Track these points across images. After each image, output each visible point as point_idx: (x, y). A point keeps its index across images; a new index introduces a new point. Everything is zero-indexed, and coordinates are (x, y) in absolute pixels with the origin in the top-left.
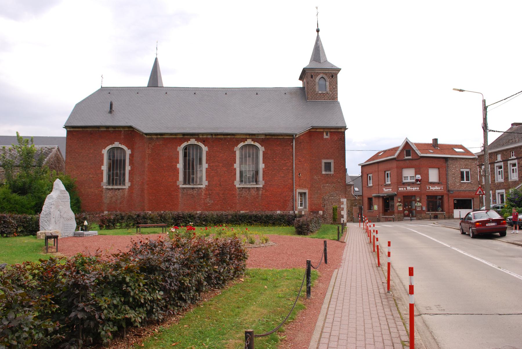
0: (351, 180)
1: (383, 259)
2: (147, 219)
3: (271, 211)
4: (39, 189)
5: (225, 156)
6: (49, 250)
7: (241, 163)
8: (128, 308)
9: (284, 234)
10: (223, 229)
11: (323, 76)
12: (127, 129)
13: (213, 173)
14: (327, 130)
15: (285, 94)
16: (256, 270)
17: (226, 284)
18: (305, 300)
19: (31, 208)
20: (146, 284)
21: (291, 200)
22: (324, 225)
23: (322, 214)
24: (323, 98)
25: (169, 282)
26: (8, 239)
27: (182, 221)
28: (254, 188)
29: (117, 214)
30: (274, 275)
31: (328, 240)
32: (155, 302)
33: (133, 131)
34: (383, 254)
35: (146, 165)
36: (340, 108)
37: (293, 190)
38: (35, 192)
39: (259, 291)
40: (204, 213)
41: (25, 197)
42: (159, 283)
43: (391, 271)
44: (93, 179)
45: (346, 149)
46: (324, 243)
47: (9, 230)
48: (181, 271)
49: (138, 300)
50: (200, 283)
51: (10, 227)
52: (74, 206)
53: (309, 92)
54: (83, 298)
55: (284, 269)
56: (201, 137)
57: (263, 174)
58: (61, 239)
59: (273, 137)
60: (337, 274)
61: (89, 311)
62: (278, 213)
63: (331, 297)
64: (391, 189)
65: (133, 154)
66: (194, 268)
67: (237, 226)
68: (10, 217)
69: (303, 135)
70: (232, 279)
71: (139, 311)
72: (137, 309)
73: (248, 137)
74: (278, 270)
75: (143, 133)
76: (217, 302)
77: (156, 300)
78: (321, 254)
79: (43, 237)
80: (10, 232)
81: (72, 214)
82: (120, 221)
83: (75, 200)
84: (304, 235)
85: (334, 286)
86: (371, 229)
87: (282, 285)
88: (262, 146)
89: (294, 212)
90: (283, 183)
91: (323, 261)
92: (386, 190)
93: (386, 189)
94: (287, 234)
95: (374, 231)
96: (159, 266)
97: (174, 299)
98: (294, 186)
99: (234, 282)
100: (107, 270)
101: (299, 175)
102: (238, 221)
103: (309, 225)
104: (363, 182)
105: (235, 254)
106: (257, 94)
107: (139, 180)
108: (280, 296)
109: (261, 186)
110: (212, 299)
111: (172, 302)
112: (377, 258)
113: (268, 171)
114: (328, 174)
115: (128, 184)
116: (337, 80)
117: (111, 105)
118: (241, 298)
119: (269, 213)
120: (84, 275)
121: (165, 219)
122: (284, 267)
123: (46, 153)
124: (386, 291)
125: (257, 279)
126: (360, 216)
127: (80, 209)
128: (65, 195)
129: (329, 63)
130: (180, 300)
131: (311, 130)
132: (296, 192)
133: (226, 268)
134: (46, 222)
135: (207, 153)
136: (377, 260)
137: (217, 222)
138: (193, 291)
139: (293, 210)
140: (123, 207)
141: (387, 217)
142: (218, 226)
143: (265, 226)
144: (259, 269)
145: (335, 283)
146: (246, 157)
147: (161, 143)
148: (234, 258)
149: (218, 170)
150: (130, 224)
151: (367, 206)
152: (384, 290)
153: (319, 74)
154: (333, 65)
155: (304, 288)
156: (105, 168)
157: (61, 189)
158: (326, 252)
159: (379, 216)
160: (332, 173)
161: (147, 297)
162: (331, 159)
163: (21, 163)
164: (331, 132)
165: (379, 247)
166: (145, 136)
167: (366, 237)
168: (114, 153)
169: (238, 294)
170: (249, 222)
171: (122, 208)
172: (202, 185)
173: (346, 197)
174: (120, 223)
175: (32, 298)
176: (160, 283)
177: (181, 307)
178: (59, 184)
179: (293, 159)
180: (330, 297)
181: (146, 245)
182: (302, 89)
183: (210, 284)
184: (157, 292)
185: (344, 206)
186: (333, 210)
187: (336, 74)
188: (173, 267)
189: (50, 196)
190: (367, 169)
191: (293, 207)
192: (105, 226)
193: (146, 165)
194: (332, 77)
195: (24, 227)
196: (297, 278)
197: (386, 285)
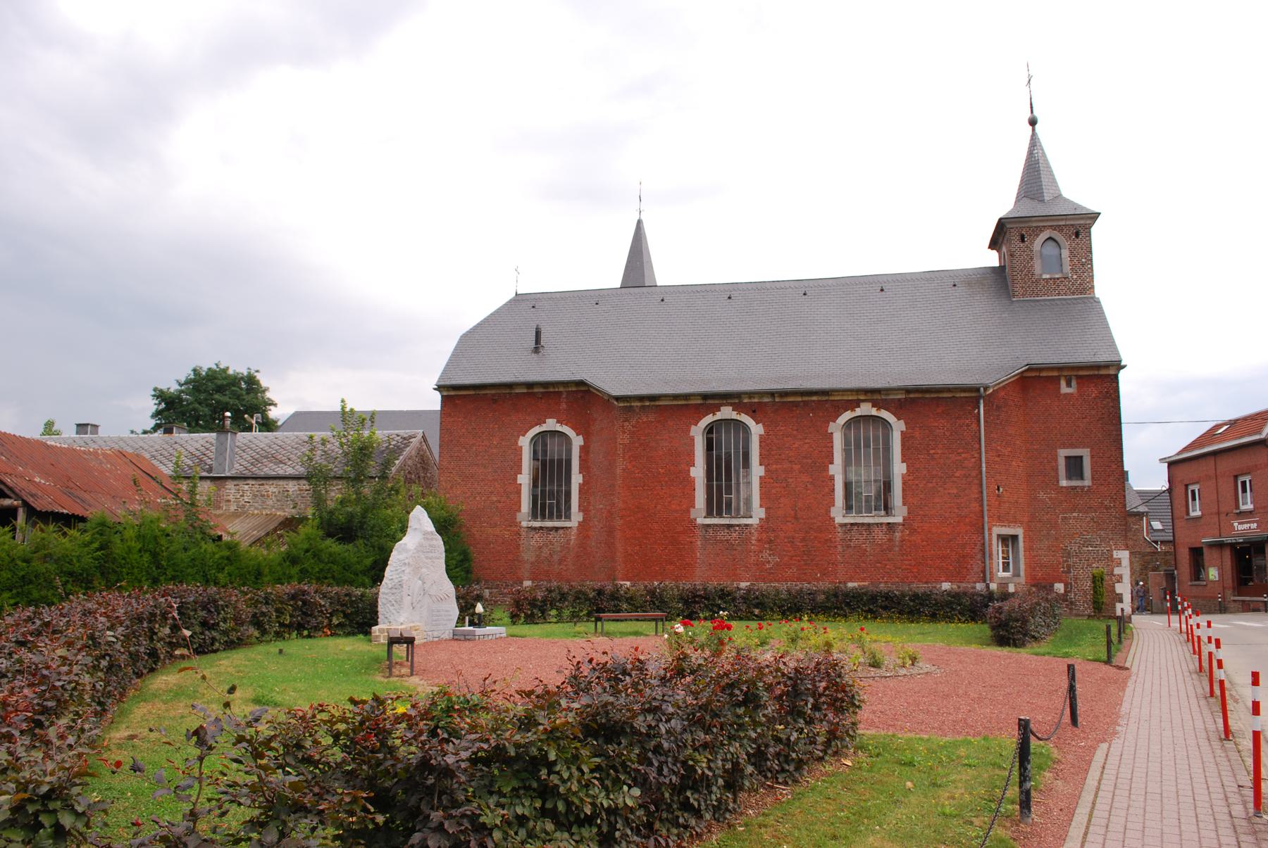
0: (1141, 502)
1: (1240, 719)
2: (620, 601)
3: (926, 583)
4: (381, 529)
5: (806, 446)
6: (394, 670)
7: (847, 463)
8: (550, 826)
9: (961, 644)
10: (803, 629)
11: (1053, 236)
12: (574, 389)
13: (778, 489)
14: (1069, 373)
15: (955, 285)
16: (884, 739)
17: (805, 773)
18: (1017, 825)
19: (364, 573)
20: (597, 768)
21: (979, 556)
22: (1069, 621)
23: (1062, 591)
24: (1055, 290)
25: (656, 764)
26: (310, 641)
27: (702, 605)
28: (881, 524)
29: (550, 587)
30: (931, 751)
31: (1080, 660)
32: (619, 815)
33: (588, 391)
34: (1237, 703)
35: (619, 471)
36: (1103, 313)
37: (983, 528)
38: (372, 536)
39: (892, 796)
40: (756, 588)
41: (350, 547)
42: (631, 768)
43: (1262, 753)
44: (499, 505)
45: (1122, 421)
46: (1069, 670)
47: (313, 622)
48: (687, 736)
49: (577, 807)
50: (736, 771)
51: (317, 614)
52: (456, 568)
53: (1015, 277)
54: (443, 797)
55: (961, 738)
56: (746, 401)
57: (904, 490)
58: (424, 645)
59: (927, 396)
60: (1107, 755)
61: (453, 832)
62: (943, 588)
63: (1089, 820)
64: (1255, 525)
65: (589, 447)
66: (722, 729)
67: (839, 621)
68: (316, 592)
69: (1004, 387)
70: (820, 759)
71: (581, 834)
72: (574, 829)
73: (862, 397)
74: (943, 740)
75: (609, 395)
76: (781, 820)
77: (622, 809)
78: (1060, 700)
79: (384, 640)
80: (315, 627)
81: (449, 588)
82: (557, 604)
83: (460, 554)
84: (1016, 646)
85: (1098, 789)
86: (1203, 633)
87: (954, 782)
88: (899, 419)
89: (988, 586)
90: (957, 511)
91: (1067, 718)
92: (1241, 527)
93: (1239, 523)
94: (969, 642)
95: (1210, 639)
96: (632, 725)
97: (670, 806)
98: (986, 519)
99: (827, 769)
100: (502, 730)
101: (998, 489)
102: (842, 609)
103: (1027, 621)
104: (1175, 507)
105: (826, 696)
106: (882, 290)
107: (601, 506)
108: (947, 811)
109: (899, 519)
110: (766, 811)
111: (664, 815)
112: (1221, 714)
113: (917, 482)
114: (1076, 487)
115: (576, 517)
116: (1090, 243)
117: (538, 334)
118: (843, 811)
119: (921, 587)
120: (447, 741)
121: (662, 601)
122: (959, 733)
123: (398, 447)
124: (1252, 811)
125: (887, 762)
126: (1168, 597)
127: (469, 576)
128: (434, 542)
129: (1066, 200)
130: (686, 811)
131: (1025, 375)
132: (990, 534)
133: (806, 731)
134: (393, 605)
135: (762, 440)
136: (1220, 721)
137: (789, 609)
138: (719, 788)
139: (984, 581)
140: (566, 571)
141: (1248, 598)
142: (791, 620)
143: (912, 622)
144: (894, 736)
145: (1100, 781)
146: (858, 447)
147: (652, 417)
148: (825, 706)
149: (790, 480)
150: (582, 611)
151: (1188, 570)
152: (1246, 808)
153: (1041, 231)
154: (1077, 206)
155: (1013, 792)
156: (524, 479)
157: (426, 528)
158: (1074, 694)
159: (1223, 597)
160: (1087, 482)
161: (599, 800)
162: (1083, 447)
163: (347, 473)
164: (1078, 377)
165: (1227, 685)
166: (616, 403)
167: (1188, 655)
168: (545, 445)
169: (834, 800)
170: (870, 611)
171: (564, 573)
172: (751, 517)
173: (1127, 548)
174: (557, 610)
175: (328, 792)
176: (633, 766)
177: (686, 827)
178: (421, 517)
179: (980, 449)
180: (1086, 820)
181: (602, 668)
182: (999, 271)
183: (764, 771)
184: (625, 788)
185: (1124, 570)
186: (1094, 582)
187: (1088, 229)
188: (668, 726)
189: (401, 545)
190: (1183, 473)
191: (984, 572)
192: (523, 615)
193: (619, 471)
194: (1077, 235)
195: (346, 616)
196: (994, 765)
197: (1250, 793)
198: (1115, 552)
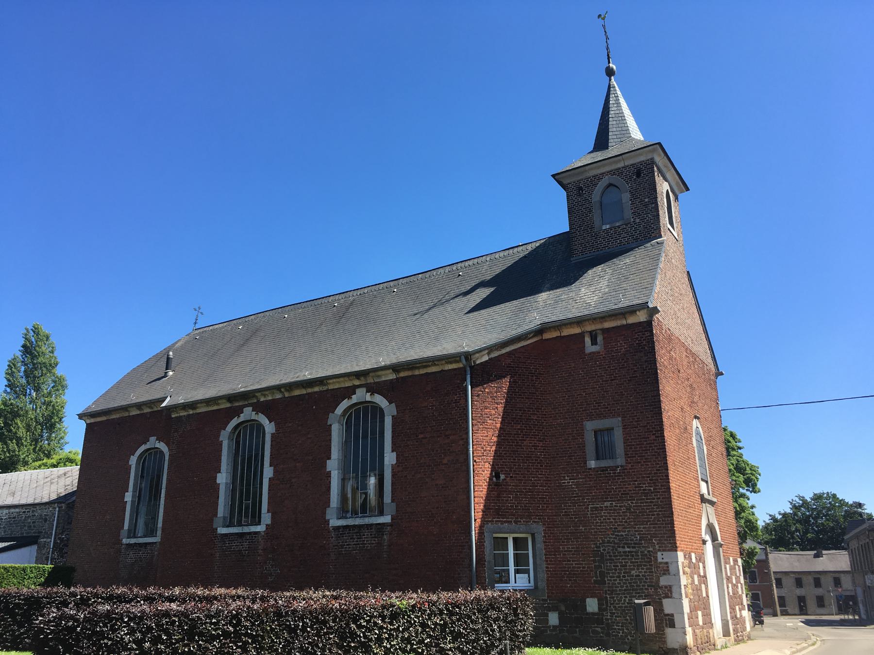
28: (372, 525)
73: (357, 383)
149: (293, 480)
162: (614, 416)
164: (605, 331)
198: (659, 554)
